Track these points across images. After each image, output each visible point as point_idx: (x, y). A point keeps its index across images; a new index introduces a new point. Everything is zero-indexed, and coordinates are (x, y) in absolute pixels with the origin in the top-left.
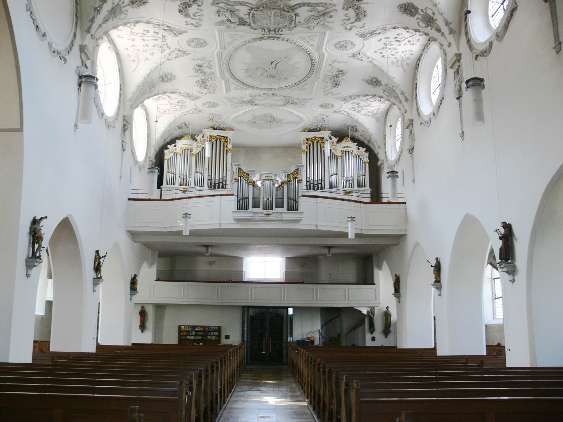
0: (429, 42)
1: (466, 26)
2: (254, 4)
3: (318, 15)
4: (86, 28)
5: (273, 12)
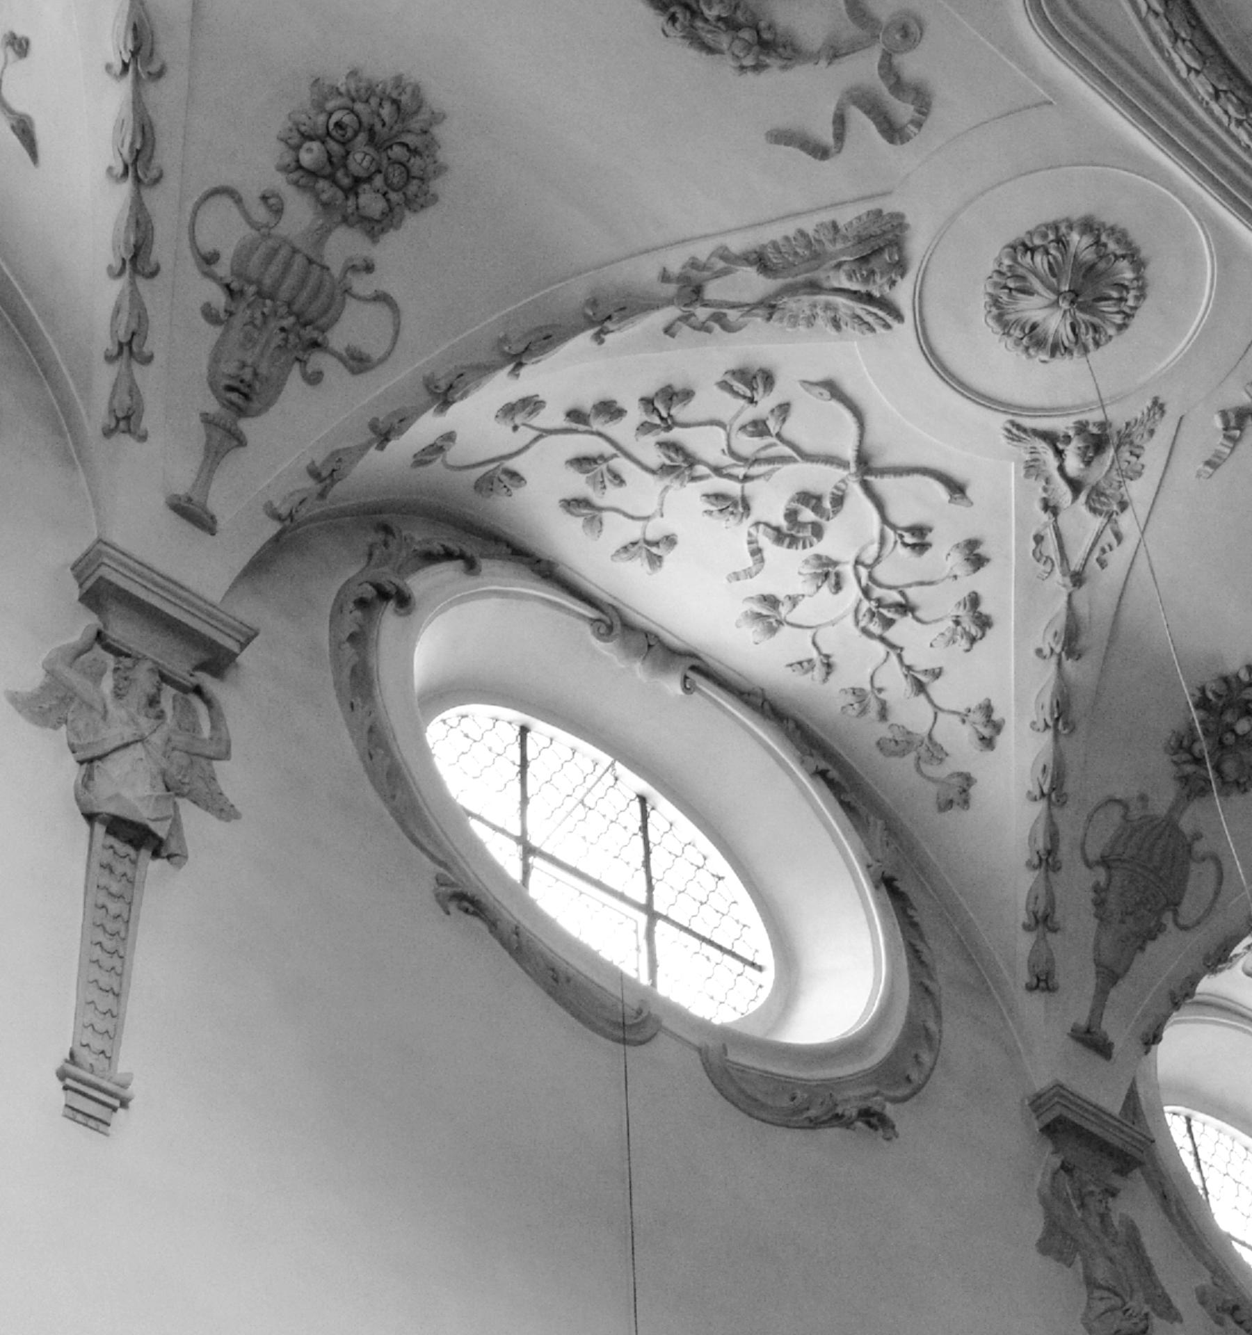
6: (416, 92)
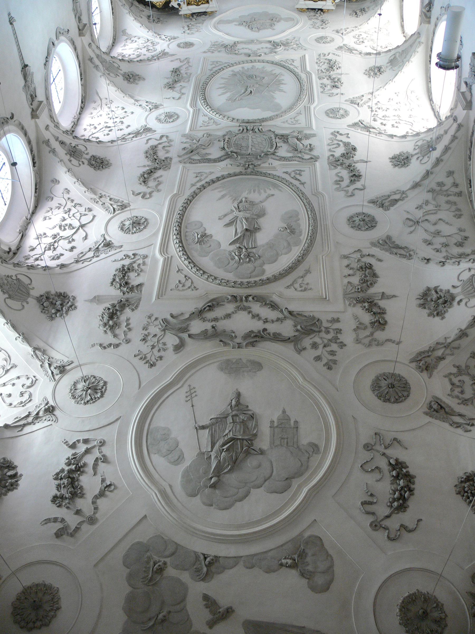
0: (73, 129)
1: (31, 151)
2: (270, 159)
3: (198, 150)
4: (462, 130)
5: (249, 151)
6: (111, 166)
